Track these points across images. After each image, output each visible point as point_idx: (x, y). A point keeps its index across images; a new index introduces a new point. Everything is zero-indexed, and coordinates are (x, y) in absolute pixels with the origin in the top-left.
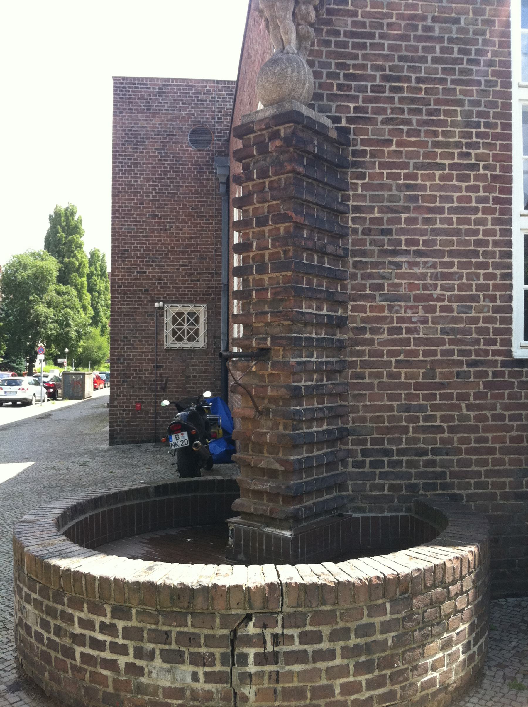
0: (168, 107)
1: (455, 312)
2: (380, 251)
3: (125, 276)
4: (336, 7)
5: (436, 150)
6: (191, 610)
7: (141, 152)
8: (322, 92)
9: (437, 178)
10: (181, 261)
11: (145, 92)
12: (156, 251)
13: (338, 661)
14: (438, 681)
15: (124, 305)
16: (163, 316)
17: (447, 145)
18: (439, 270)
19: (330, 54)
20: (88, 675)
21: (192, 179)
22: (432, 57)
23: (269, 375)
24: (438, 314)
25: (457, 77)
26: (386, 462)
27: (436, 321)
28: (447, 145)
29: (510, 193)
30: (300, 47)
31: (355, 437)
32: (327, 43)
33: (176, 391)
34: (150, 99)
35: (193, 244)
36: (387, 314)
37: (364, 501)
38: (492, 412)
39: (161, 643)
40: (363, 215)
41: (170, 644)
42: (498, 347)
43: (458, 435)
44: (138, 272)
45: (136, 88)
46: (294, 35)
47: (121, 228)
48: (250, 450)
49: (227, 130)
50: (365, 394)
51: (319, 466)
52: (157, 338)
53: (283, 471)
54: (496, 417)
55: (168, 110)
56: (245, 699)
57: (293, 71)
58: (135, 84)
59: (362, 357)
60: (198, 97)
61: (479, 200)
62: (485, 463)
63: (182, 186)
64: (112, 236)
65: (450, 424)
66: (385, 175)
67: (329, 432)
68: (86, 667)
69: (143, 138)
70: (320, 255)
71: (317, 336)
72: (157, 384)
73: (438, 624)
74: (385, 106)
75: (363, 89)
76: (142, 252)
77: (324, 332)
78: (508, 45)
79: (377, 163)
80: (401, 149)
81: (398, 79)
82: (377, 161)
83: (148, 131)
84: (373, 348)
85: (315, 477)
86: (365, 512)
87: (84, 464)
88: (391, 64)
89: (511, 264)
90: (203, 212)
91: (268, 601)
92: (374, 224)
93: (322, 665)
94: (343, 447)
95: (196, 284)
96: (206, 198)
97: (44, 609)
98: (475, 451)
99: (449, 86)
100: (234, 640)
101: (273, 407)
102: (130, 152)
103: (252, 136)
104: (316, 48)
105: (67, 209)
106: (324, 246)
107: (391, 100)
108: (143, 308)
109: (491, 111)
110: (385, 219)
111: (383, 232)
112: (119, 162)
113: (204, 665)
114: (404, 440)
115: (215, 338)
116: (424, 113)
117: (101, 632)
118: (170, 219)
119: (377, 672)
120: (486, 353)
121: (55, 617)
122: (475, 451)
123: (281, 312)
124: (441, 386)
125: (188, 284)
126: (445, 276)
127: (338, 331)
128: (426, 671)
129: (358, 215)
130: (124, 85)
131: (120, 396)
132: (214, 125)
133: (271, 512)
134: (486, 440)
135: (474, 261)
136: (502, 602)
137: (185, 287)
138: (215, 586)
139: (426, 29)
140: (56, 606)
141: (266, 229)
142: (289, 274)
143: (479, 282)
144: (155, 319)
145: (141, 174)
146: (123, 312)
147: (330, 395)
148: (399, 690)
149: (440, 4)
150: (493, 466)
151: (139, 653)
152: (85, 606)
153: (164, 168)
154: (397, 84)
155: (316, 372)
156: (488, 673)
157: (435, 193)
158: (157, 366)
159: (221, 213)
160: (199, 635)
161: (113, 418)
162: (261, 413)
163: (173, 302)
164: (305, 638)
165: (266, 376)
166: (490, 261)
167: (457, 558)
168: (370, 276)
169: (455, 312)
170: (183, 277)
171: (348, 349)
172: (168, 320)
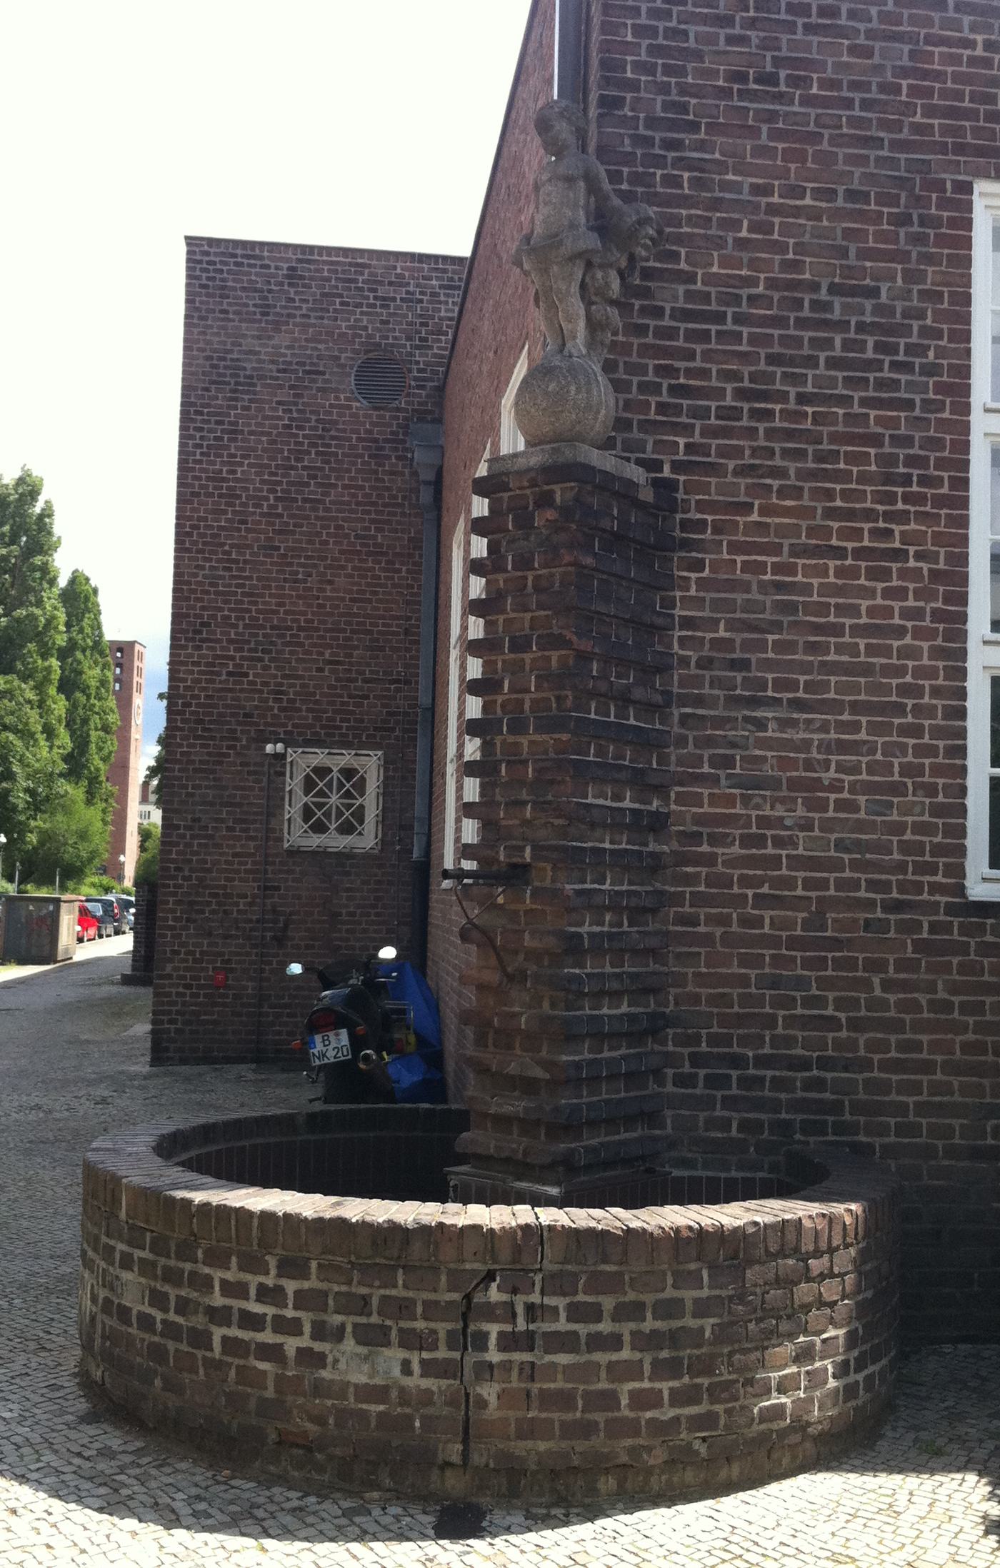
0: (308, 309)
1: (863, 812)
2: (727, 698)
3: (199, 681)
4: (658, 265)
5: (831, 523)
6: (402, 1262)
7: (244, 408)
8: (630, 416)
9: (831, 572)
10: (327, 653)
11: (257, 274)
12: (272, 628)
13: (625, 1354)
14: (788, 1412)
15: (194, 746)
16: (284, 774)
17: (850, 514)
18: (833, 735)
19: (645, 350)
20: (233, 1373)
21: (358, 471)
22: (827, 358)
23: (526, 912)
24: (831, 814)
25: (871, 394)
26: (734, 1077)
27: (827, 826)
28: (850, 514)
29: (964, 602)
30: (592, 343)
31: (679, 1031)
32: (641, 330)
33: (307, 947)
34: (270, 291)
35: (357, 615)
36: (739, 810)
37: (694, 1149)
38: (929, 996)
39: (356, 1314)
40: (700, 634)
41: (370, 1315)
42: (939, 878)
43: (867, 1035)
44: (229, 674)
45: (236, 264)
46: (582, 324)
47: (196, 575)
48: (490, 1042)
49: (440, 364)
50: (700, 953)
51: (611, 1077)
52: (268, 822)
53: (548, 1082)
54: (935, 1006)
55: (308, 317)
56: (482, 1404)
57: (578, 390)
58: (235, 256)
59: (694, 886)
60: (375, 290)
61: (907, 614)
62: (915, 1088)
63: (335, 486)
64: (175, 591)
65: (851, 1014)
66: (739, 565)
67: (632, 1018)
68: (229, 1359)
69: (251, 377)
70: (620, 703)
71: (612, 847)
72: (265, 929)
73: (789, 1317)
74: (741, 443)
75: (703, 413)
76: (241, 630)
77: (625, 839)
78: (966, 336)
79: (725, 543)
80: (768, 520)
81: (764, 396)
82: (725, 540)
83: (264, 361)
84: (714, 870)
85: (605, 1096)
86: (694, 1168)
87: (104, 1101)
88: (753, 368)
89: (965, 729)
90: (381, 546)
91: (520, 1252)
92: (719, 650)
93: (602, 1357)
94: (657, 1047)
95: (361, 705)
96: (389, 514)
97: (159, 1272)
98: (896, 1066)
99: (856, 409)
100: (467, 1310)
101: (532, 969)
102: (221, 407)
103: (506, 495)
104: (621, 338)
105: (21, 481)
106: (628, 688)
107: (751, 433)
108: (238, 754)
109: (932, 456)
110: (738, 641)
111: (736, 665)
112: (195, 429)
113: (421, 1349)
114: (767, 1039)
115: (402, 827)
116: (810, 457)
117: (258, 1300)
118: (307, 557)
119: (686, 1379)
120: (918, 887)
121: (178, 1284)
122: (896, 1066)
123: (549, 803)
124: (836, 944)
125: (343, 704)
126: (843, 747)
127: (651, 839)
128: (769, 1391)
129: (690, 633)
130: (212, 258)
131: (178, 953)
132: (411, 354)
133: (526, 1154)
134: (917, 1046)
135: (896, 721)
136: (947, 1348)
137: (334, 711)
138: (441, 1225)
139: (817, 305)
140: (181, 1265)
141: (528, 657)
142: (565, 737)
143: (905, 760)
144: (265, 779)
145: (243, 456)
146: (193, 762)
147: (635, 952)
148: (722, 1413)
149: (844, 262)
150: (930, 1095)
151: (320, 1332)
152: (234, 1259)
153: (296, 443)
154: (762, 405)
155: (608, 909)
156: (890, 1434)
157: (828, 600)
158: (266, 888)
159: (421, 548)
160: (413, 1302)
161: (163, 1004)
162: (511, 978)
163: (308, 743)
164: (576, 1312)
165: (522, 913)
166: (927, 723)
167: (824, 1215)
168: (710, 742)
169: (863, 812)
170: (330, 687)
171: (669, 871)
172: (294, 783)
